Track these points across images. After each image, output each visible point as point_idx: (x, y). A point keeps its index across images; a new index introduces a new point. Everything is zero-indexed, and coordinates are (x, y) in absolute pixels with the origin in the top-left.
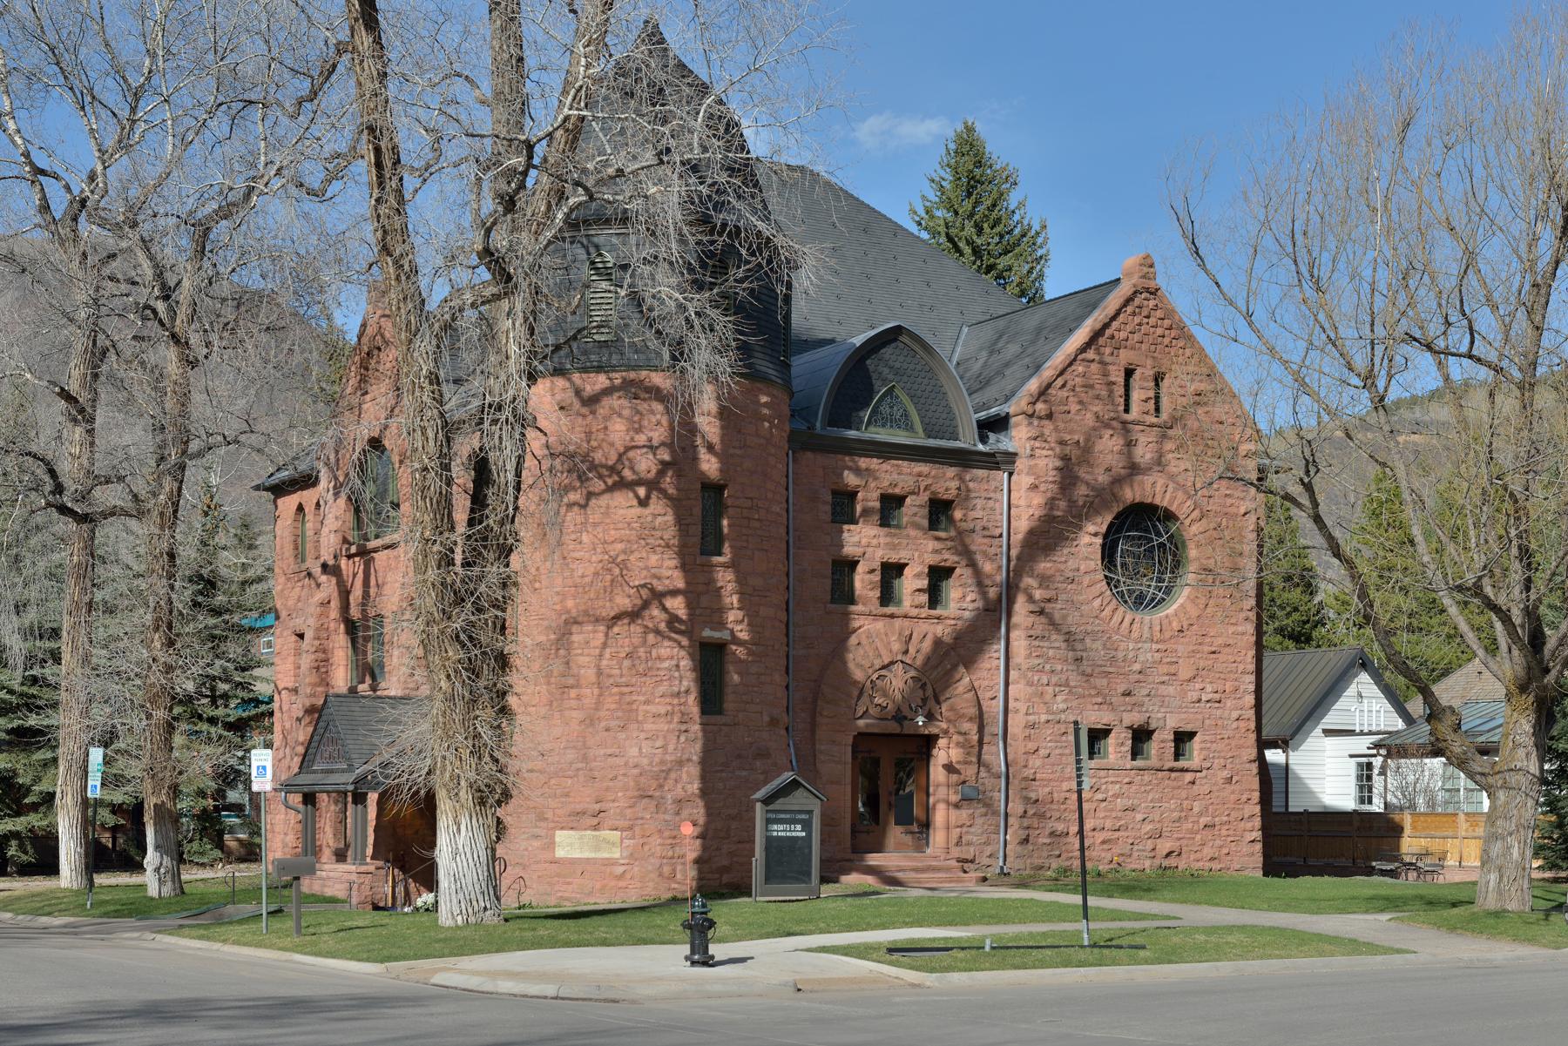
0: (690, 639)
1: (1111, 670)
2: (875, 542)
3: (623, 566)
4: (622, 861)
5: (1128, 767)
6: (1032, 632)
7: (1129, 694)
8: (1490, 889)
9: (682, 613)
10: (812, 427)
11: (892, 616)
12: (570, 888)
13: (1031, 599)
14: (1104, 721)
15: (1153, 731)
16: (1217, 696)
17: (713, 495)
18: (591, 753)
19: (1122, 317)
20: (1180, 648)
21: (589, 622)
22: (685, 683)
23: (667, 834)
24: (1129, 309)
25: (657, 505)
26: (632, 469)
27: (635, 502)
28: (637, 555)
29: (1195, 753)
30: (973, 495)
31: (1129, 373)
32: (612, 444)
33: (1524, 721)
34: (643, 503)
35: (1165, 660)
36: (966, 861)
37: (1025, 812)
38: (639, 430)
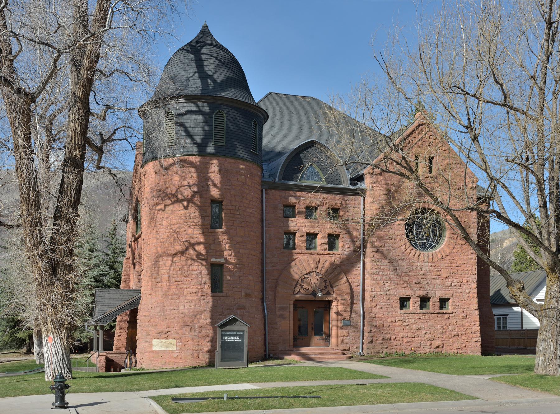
0: (206, 262)
1: (410, 274)
2: (303, 225)
3: (178, 233)
4: (177, 352)
5: (418, 312)
6: (373, 259)
7: (418, 283)
8: (540, 364)
9: (203, 252)
10: (275, 180)
11: (311, 254)
12: (157, 362)
13: (373, 246)
14: (407, 294)
15: (430, 298)
16: (459, 284)
17: (218, 205)
18: (165, 308)
19: (413, 135)
20: (442, 265)
21: (165, 256)
22: (204, 280)
23: (196, 340)
24: (417, 132)
25: (192, 209)
26: (182, 194)
27: (182, 208)
28: (183, 229)
29: (450, 306)
30: (348, 206)
31: (417, 157)
32: (174, 185)
33: (555, 286)
34: (186, 208)
35: (435, 270)
36: (346, 350)
37: (371, 330)
38: (184, 180)
